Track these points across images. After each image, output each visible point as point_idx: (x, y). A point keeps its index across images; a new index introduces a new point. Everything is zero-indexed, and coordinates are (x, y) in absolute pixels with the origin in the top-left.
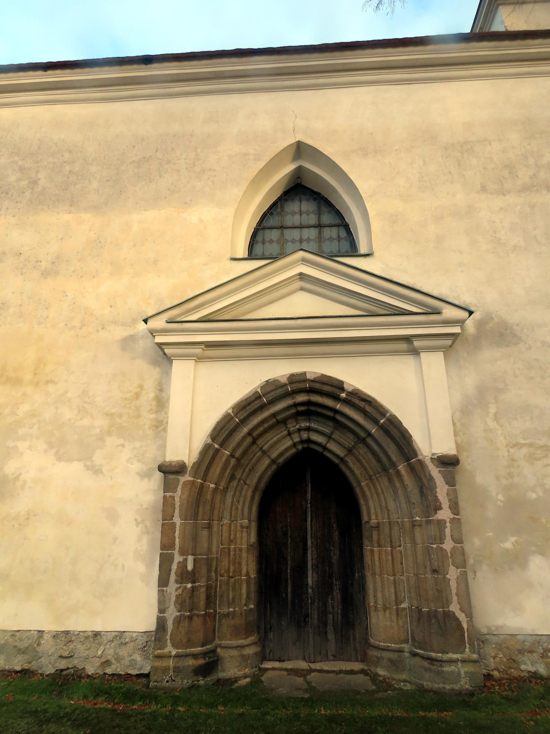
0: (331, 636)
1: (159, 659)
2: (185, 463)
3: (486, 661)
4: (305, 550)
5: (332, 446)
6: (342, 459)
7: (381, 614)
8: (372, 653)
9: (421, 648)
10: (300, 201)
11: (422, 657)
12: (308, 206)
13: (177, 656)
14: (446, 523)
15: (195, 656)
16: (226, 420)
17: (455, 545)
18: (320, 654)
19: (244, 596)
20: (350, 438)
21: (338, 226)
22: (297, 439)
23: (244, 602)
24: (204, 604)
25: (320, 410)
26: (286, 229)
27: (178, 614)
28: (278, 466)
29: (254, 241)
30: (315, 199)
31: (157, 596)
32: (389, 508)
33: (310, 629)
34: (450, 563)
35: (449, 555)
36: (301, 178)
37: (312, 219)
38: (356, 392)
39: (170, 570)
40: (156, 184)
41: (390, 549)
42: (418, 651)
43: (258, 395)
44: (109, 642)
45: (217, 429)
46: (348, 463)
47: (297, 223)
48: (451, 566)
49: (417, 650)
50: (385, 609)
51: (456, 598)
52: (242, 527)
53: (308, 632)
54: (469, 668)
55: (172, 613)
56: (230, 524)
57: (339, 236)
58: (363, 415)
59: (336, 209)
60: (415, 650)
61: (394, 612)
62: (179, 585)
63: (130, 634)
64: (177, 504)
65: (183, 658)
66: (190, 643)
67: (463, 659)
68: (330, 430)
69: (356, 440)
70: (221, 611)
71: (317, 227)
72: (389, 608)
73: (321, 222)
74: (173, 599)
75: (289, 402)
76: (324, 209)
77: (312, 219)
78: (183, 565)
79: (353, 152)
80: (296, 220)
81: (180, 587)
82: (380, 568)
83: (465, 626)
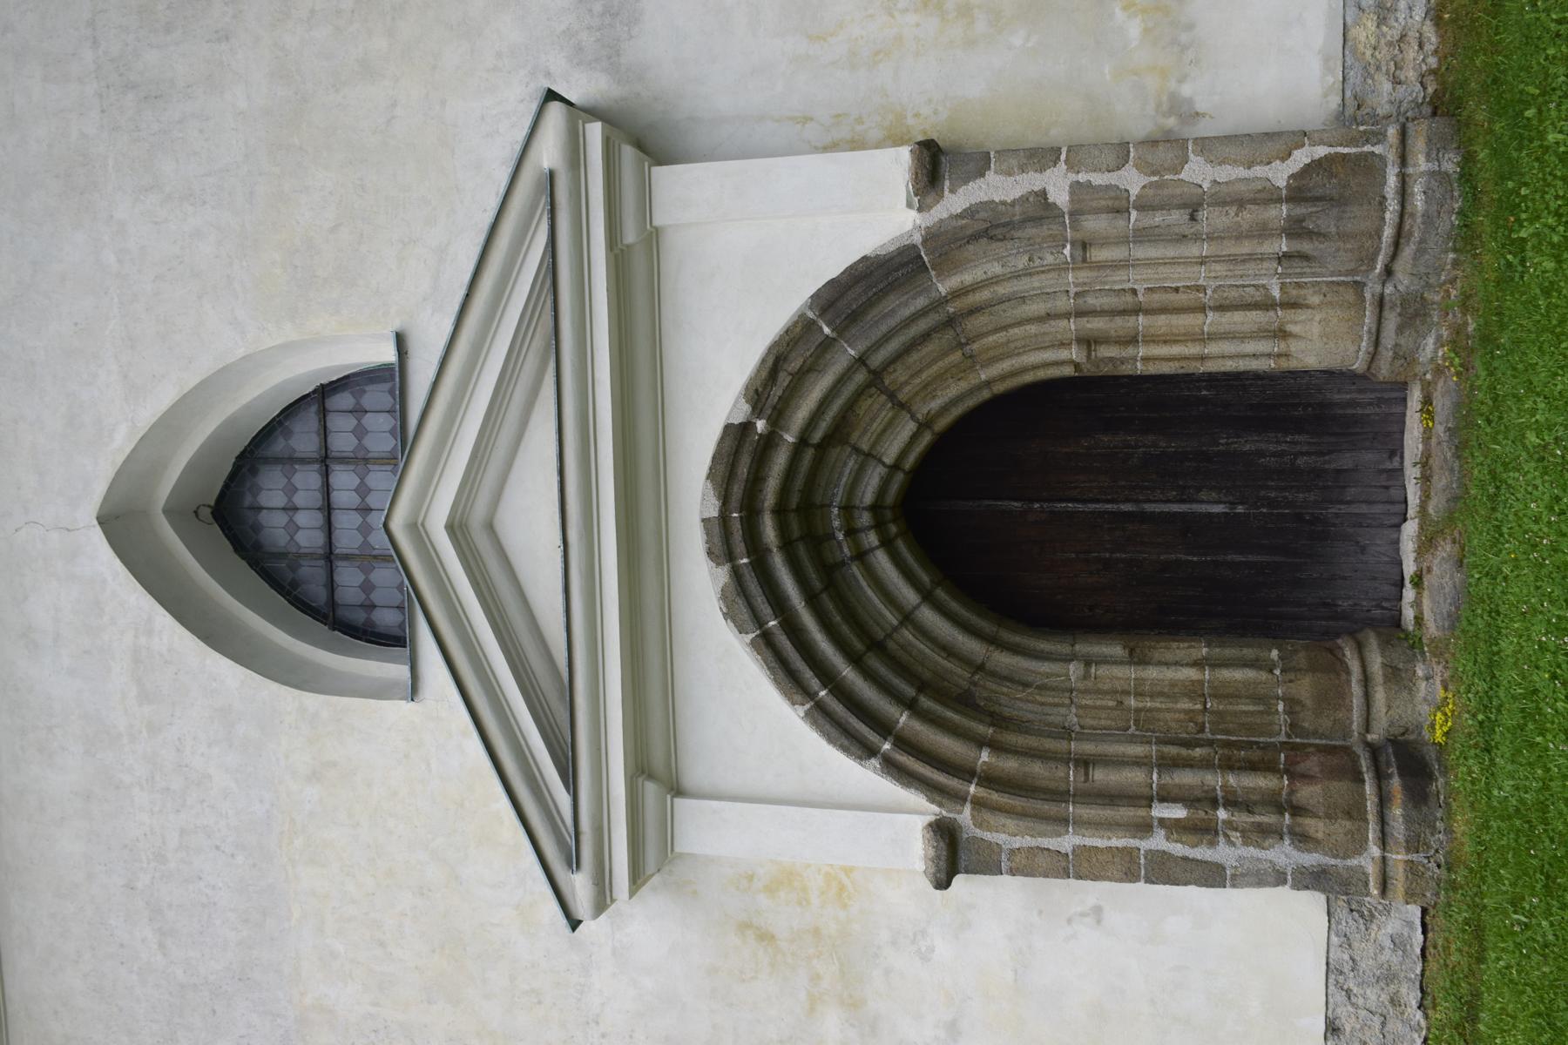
0: (1345, 461)
1: (1389, 886)
2: (930, 825)
3: (1405, 104)
4: (1143, 517)
5: (890, 453)
6: (924, 425)
7: (1294, 346)
8: (1384, 370)
9: (1373, 260)
10: (261, 508)
11: (1394, 256)
12: (271, 490)
13: (1383, 842)
14: (1078, 182)
15: (1383, 801)
16: (821, 716)
17: (1131, 163)
18: (1387, 488)
19: (1250, 674)
20: (871, 405)
21: (323, 413)
22: (872, 539)
23: (1264, 676)
24: (1265, 778)
25: (799, 483)
26: (333, 548)
27: (1287, 842)
28: (939, 584)
29: (365, 632)
30: (254, 471)
31: (1246, 889)
32: (1043, 313)
33: (1330, 511)
34: (1176, 177)
35: (1156, 178)
36: (198, 508)
37: (307, 480)
38: (752, 393)
39: (1185, 859)
40: (220, 889)
41: (1141, 318)
42: (1379, 266)
43: (760, 641)
44: (1349, 998)
45: (846, 743)
46: (933, 412)
47: (317, 519)
48: (1181, 177)
49: (1379, 267)
50: (1282, 334)
51: (1258, 168)
52: (1086, 676)
53: (1337, 515)
54: (1418, 145)
55: (1284, 854)
56: (1079, 707)
57: (350, 412)
58: (812, 376)
59: (278, 416)
60: (1377, 271)
61: (1289, 315)
62: (1221, 839)
63: (1332, 950)
64: (1028, 841)
65: (1387, 829)
66: (1355, 812)
67: (1399, 161)
68: (849, 456)
69: (873, 390)
70: (1283, 732)
71: (327, 466)
72: (1282, 324)
73: (315, 455)
74: (1252, 851)
75: (778, 561)
76: (279, 446)
77: (307, 480)
78: (1172, 827)
79: (126, 377)
80: (309, 520)
81: (1226, 836)
82: (1186, 341)
83: (1321, 151)
